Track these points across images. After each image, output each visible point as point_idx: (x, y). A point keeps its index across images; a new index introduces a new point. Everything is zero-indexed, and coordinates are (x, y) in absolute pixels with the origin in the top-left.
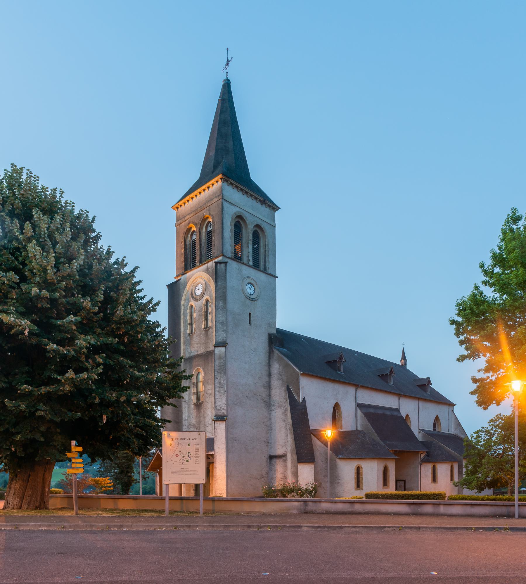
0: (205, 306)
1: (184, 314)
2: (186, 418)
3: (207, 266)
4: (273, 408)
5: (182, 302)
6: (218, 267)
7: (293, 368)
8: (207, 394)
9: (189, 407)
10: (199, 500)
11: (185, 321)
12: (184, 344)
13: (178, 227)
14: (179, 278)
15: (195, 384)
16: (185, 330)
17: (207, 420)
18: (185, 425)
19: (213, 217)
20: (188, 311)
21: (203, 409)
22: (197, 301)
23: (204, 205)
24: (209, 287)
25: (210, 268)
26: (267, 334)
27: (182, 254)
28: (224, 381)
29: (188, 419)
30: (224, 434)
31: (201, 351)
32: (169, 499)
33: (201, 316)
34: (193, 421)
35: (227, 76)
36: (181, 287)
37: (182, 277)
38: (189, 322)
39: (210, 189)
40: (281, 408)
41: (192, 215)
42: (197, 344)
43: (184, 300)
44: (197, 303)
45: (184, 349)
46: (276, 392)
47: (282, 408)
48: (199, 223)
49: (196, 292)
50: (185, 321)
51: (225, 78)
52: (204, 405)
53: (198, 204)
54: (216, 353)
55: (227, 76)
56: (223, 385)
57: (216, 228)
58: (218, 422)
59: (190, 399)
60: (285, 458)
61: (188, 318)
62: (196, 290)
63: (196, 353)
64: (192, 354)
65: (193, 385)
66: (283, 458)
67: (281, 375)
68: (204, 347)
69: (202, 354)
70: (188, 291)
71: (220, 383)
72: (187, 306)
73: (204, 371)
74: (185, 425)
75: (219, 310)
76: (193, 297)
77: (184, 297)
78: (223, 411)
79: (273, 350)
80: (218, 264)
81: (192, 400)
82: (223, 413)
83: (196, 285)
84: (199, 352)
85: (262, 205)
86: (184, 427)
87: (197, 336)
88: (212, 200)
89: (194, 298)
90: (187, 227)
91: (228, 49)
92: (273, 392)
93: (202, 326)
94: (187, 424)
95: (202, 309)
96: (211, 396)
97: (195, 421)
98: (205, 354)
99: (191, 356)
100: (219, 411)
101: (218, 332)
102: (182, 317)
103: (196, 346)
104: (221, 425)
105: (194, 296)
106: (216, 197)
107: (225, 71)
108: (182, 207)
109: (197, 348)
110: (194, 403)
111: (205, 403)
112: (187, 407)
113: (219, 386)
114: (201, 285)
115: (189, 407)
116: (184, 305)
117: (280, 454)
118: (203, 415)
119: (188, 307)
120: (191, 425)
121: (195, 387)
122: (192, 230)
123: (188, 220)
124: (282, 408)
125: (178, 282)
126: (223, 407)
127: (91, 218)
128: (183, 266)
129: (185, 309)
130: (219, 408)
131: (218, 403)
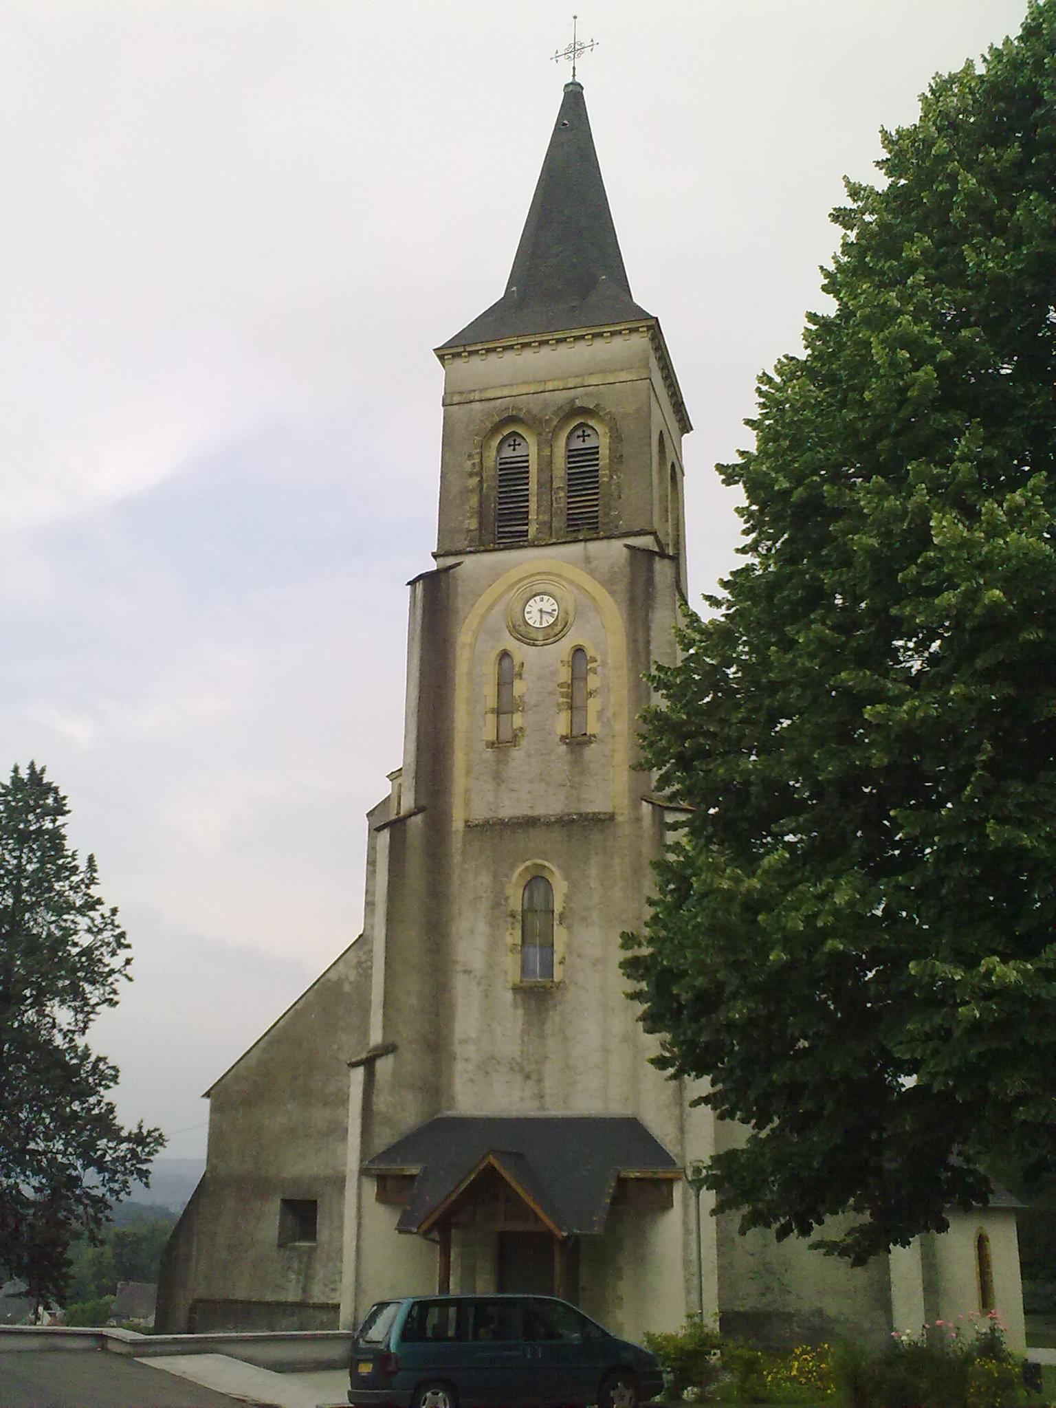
2: (473, 1035)
8: (579, 956)
14: (451, 561)
18: (467, 1060)
21: (559, 1008)
31: (552, 805)
38: (492, 702)
42: (531, 782)
65: (510, 919)
73: (567, 877)
80: (657, 559)
91: (575, 17)
121: (518, 926)
125: (451, 571)
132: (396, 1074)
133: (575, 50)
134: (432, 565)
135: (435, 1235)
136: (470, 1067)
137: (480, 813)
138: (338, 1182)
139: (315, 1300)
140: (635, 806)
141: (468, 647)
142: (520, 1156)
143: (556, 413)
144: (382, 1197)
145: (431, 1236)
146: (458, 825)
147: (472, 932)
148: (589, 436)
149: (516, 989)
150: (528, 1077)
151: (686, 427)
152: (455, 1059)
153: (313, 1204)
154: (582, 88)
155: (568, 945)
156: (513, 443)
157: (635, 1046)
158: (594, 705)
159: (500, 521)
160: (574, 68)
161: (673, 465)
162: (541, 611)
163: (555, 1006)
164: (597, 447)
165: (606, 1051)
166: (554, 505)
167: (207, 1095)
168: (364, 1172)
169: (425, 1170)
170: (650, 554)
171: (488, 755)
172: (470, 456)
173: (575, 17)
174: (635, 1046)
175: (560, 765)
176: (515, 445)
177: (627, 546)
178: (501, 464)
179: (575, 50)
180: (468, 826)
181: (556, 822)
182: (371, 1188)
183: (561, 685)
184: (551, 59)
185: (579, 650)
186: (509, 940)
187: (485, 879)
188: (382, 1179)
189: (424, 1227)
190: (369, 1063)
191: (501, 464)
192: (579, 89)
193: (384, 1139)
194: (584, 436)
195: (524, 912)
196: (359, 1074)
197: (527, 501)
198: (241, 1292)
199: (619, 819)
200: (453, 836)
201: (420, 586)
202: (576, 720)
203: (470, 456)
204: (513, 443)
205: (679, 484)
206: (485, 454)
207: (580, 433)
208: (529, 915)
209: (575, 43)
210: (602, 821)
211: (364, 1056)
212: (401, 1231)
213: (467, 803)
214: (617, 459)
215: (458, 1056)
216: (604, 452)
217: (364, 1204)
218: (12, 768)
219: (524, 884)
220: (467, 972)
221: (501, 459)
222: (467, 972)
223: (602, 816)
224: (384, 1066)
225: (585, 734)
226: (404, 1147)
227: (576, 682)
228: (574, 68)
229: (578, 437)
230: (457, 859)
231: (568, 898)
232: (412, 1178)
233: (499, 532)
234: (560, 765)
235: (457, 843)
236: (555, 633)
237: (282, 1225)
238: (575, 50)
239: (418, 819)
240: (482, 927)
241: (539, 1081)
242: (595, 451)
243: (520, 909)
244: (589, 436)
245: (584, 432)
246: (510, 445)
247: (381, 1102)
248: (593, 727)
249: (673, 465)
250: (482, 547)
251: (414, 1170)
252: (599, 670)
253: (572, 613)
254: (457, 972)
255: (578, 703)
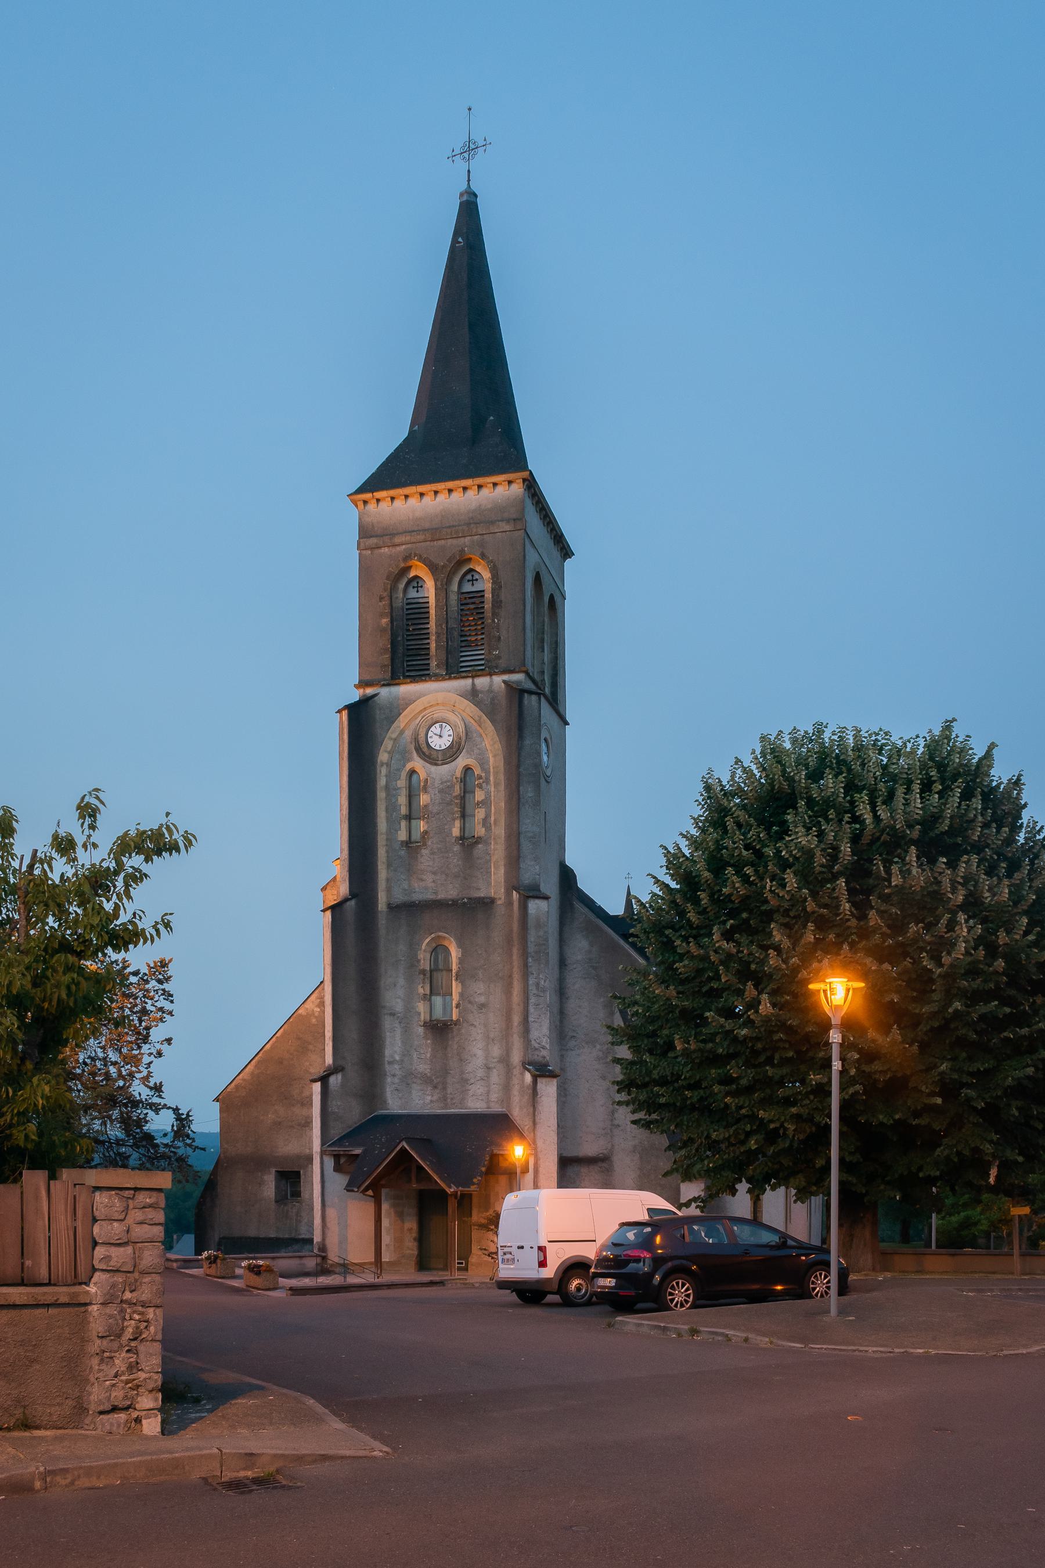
0: (461, 782)
1: (387, 787)
2: (397, 1058)
3: (473, 684)
4: (572, 1043)
5: (383, 757)
6: (526, 702)
7: (630, 955)
8: (470, 1002)
9: (407, 1031)
10: (1013, 1255)
11: (392, 808)
12: (389, 865)
13: (364, 552)
14: (370, 691)
15: (428, 975)
16: (393, 829)
17: (469, 1068)
18: (394, 1076)
19: (495, 566)
20: (402, 783)
21: (456, 1039)
22: (436, 765)
23: (465, 527)
24: (478, 739)
25: (482, 692)
26: (558, 862)
27: (383, 630)
28: (545, 981)
29: (402, 1061)
30: (554, 1108)
31: (450, 892)
32: (1021, 1255)
33: (449, 804)
34: (423, 1068)
35: (469, 180)
36: (379, 715)
37: (385, 692)
38: (404, 810)
39: (481, 493)
40: (595, 1047)
41: (421, 537)
42: (434, 873)
43: (389, 753)
44: (433, 768)
45: (388, 880)
46: (580, 1007)
47: (598, 1047)
48: (443, 567)
49: (430, 740)
50: (392, 808)
51: (464, 187)
52: (459, 1030)
53: (442, 516)
54: (530, 912)
55: (469, 180)
56: (544, 991)
57: (503, 598)
58: (544, 1080)
59: (409, 1009)
60: (604, 1165)
61: (402, 800)
62: (430, 734)
63: (433, 897)
64: (417, 897)
65: (422, 976)
66: (600, 1164)
67: (595, 968)
68: (457, 886)
69: (453, 900)
70: (402, 732)
71: (537, 985)
72: (399, 770)
73: (460, 945)
74: (394, 1076)
75: (527, 806)
76: (418, 749)
77: (388, 744)
78: (544, 1053)
79: (572, 905)
80: (526, 695)
81: (419, 1014)
82: (544, 1057)
83: (430, 722)
84: (441, 896)
85: (555, 545)
86: (389, 1080)
87: (433, 853)
88: (492, 523)
89: (424, 753)
90: (402, 565)
91: (470, 109)
92: (572, 1005)
93: (450, 830)
94: (398, 1072)
95: (452, 786)
96: (484, 1010)
97: (429, 1067)
98: (464, 903)
99: (413, 899)
100: (537, 1053)
101: (524, 861)
102: (381, 795)
103: (429, 878)
104: (548, 1087)
105: (425, 750)
106: (508, 521)
107: (461, 165)
108: (381, 503)
109: (433, 885)
110: (425, 1023)
111: (465, 1025)
112: (398, 1032)
113: (535, 991)
114: (448, 727)
115: (407, 1031)
116: (388, 765)
117: (590, 1154)
118: (459, 1054)
119: (404, 774)
120: (416, 1077)
121: (428, 981)
122: (412, 574)
123: (404, 547)
124: (598, 1047)
125: (370, 702)
126: (543, 1044)
127: (1037, 828)
128: (388, 662)
129: (392, 777)
130: (537, 1046)
131: (534, 1034)
132: (343, 1085)
133: (469, 150)
134: (355, 696)
135: (370, 1192)
136: (396, 1080)
137: (399, 897)
138: (310, 1159)
139: (303, 1236)
140: (508, 894)
141: (385, 766)
142: (429, 1141)
143: (449, 560)
144: (338, 1168)
145: (367, 1193)
146: (382, 905)
147: (395, 985)
148: (477, 580)
149: (425, 1025)
150: (435, 1087)
151: (566, 552)
152: (386, 1075)
153: (298, 1174)
154: (476, 196)
155: (461, 995)
156: (416, 585)
157: (508, 1065)
158: (480, 814)
159: (409, 656)
160: (469, 171)
161: (552, 597)
162: (440, 736)
163: (454, 1037)
164: (483, 591)
165: (489, 1068)
166: (450, 643)
167: (217, 1099)
168: (323, 1153)
169: (364, 1152)
170: (522, 692)
171: (403, 852)
172: (381, 599)
173: (470, 109)
174: (508, 1065)
175: (455, 861)
176: (418, 587)
177: (504, 682)
178: (407, 604)
179: (469, 150)
180: (390, 906)
181: (452, 905)
182: (330, 1162)
183: (456, 797)
184: (448, 158)
185: (467, 769)
186: (421, 991)
187: (402, 948)
188: (337, 1157)
189: (362, 1188)
190: (324, 1079)
191: (407, 604)
192: (472, 199)
193: (337, 1131)
194: (473, 580)
195: (431, 971)
196: (317, 1087)
197: (428, 638)
198: (252, 1232)
199: (499, 902)
200: (380, 915)
201: (345, 713)
202: (467, 825)
203: (381, 599)
204: (416, 585)
205: (559, 611)
206: (394, 596)
207: (469, 577)
208: (435, 974)
209: (469, 141)
210: (487, 904)
211: (322, 1074)
212: (348, 1191)
213: (389, 890)
214: (497, 603)
215: (388, 1074)
216: (488, 595)
217: (326, 1173)
218: (19, 819)
219: (431, 950)
220: (393, 1014)
221: (407, 599)
222: (393, 1014)
223: (485, 900)
224: (335, 1080)
225: (474, 837)
226: (352, 1135)
227: (467, 795)
228: (469, 171)
229: (469, 581)
230: (382, 931)
231: (461, 961)
232: (357, 1155)
233: (408, 666)
234: (455, 861)
235: (382, 922)
236: (452, 752)
237: (277, 1187)
238: (469, 150)
239: (353, 903)
240: (401, 981)
241: (445, 1088)
242: (481, 594)
243: (428, 969)
244: (477, 580)
245: (473, 576)
246: (414, 587)
247: (335, 1105)
248: (480, 831)
249: (552, 597)
250: (394, 680)
251: (358, 1151)
252: (484, 785)
253: (464, 738)
254: (385, 1015)
255: (468, 811)
